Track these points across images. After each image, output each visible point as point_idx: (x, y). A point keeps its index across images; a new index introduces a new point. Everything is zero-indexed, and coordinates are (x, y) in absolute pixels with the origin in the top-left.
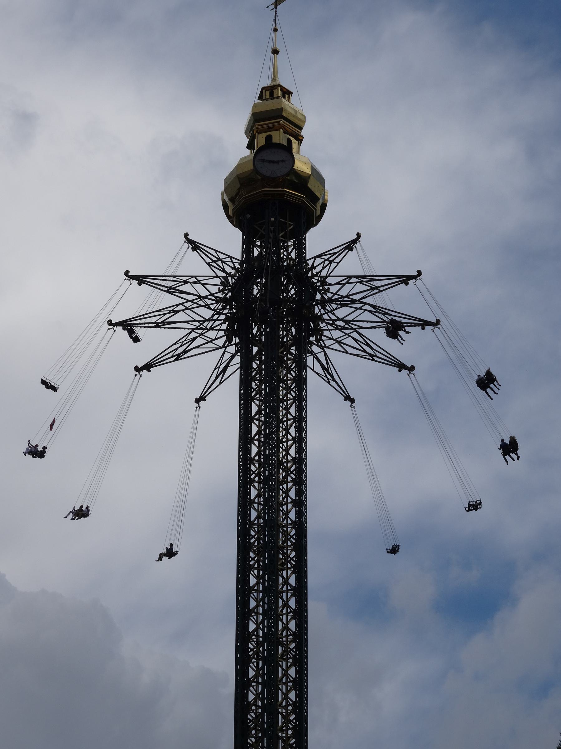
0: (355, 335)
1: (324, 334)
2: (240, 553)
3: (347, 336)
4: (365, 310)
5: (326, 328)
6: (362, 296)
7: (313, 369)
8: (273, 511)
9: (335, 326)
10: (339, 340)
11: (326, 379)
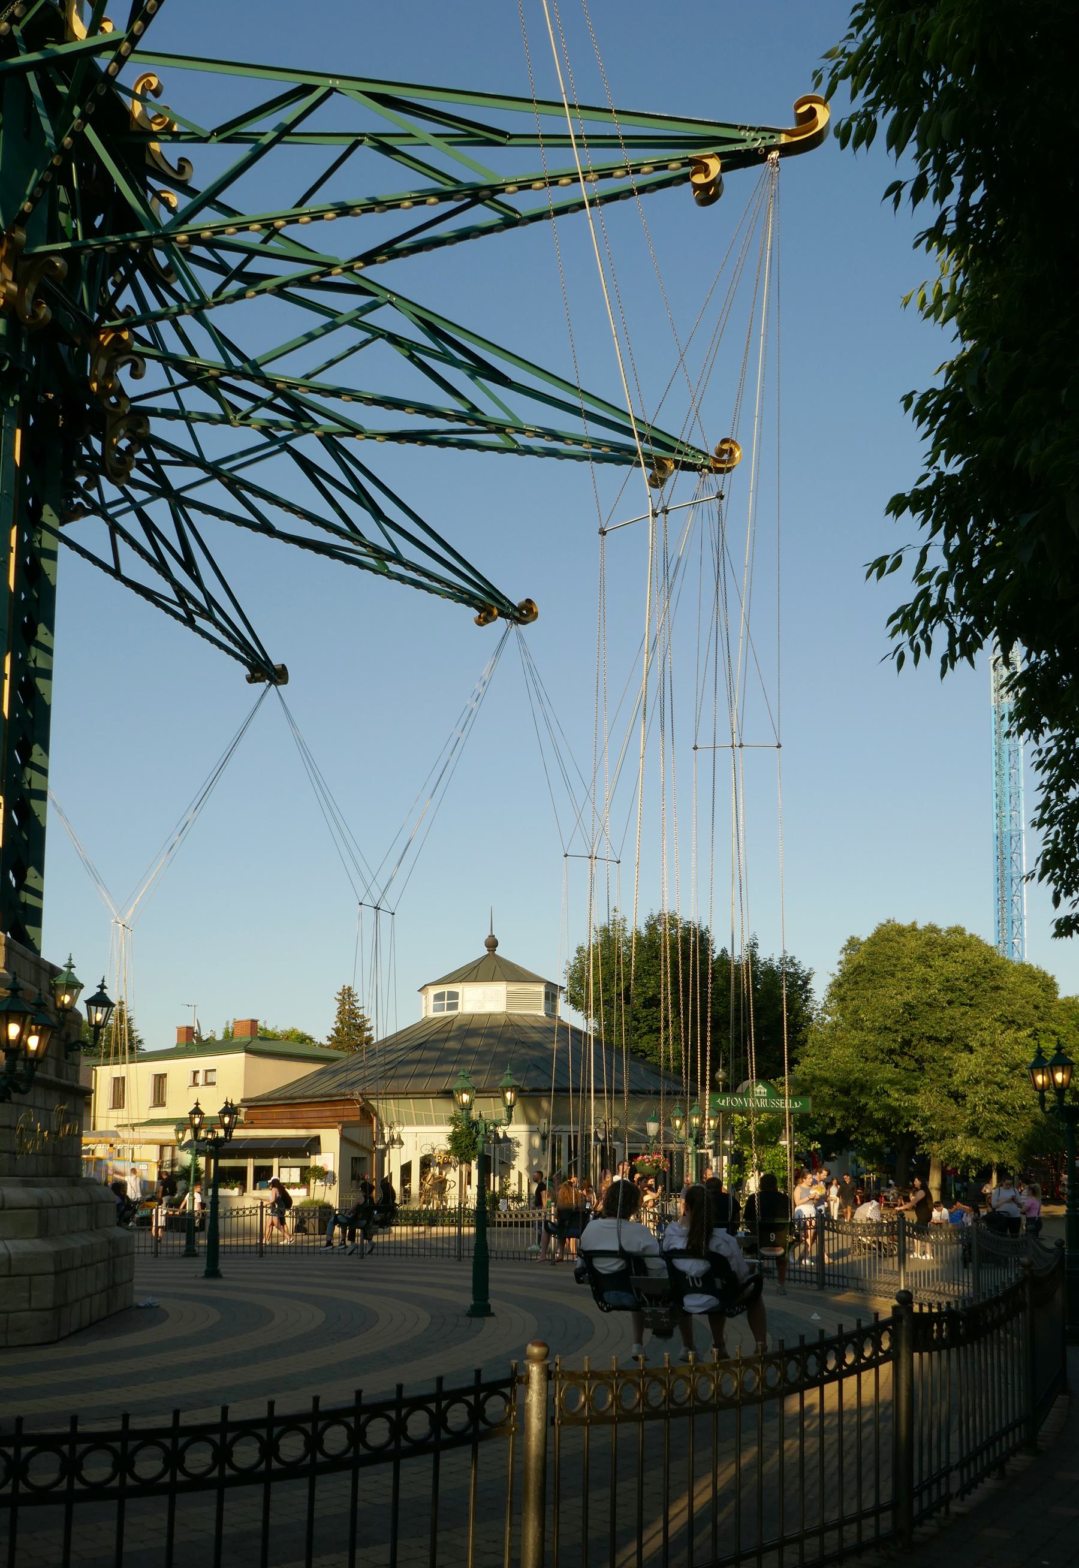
4: (377, 333)
5: (168, 402)
7: (113, 566)
11: (181, 611)
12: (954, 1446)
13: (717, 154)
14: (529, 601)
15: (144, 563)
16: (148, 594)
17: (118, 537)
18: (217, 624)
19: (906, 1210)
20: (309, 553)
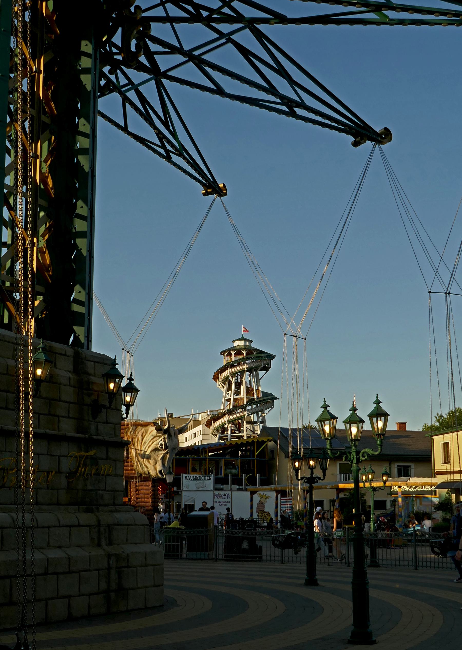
1: (100, 82)
2: (73, 242)
5: (159, 12)
9: (190, 8)
11: (162, 151)
12: (105, 473)
14: (386, 129)
17: (127, 105)
20: (318, 27)
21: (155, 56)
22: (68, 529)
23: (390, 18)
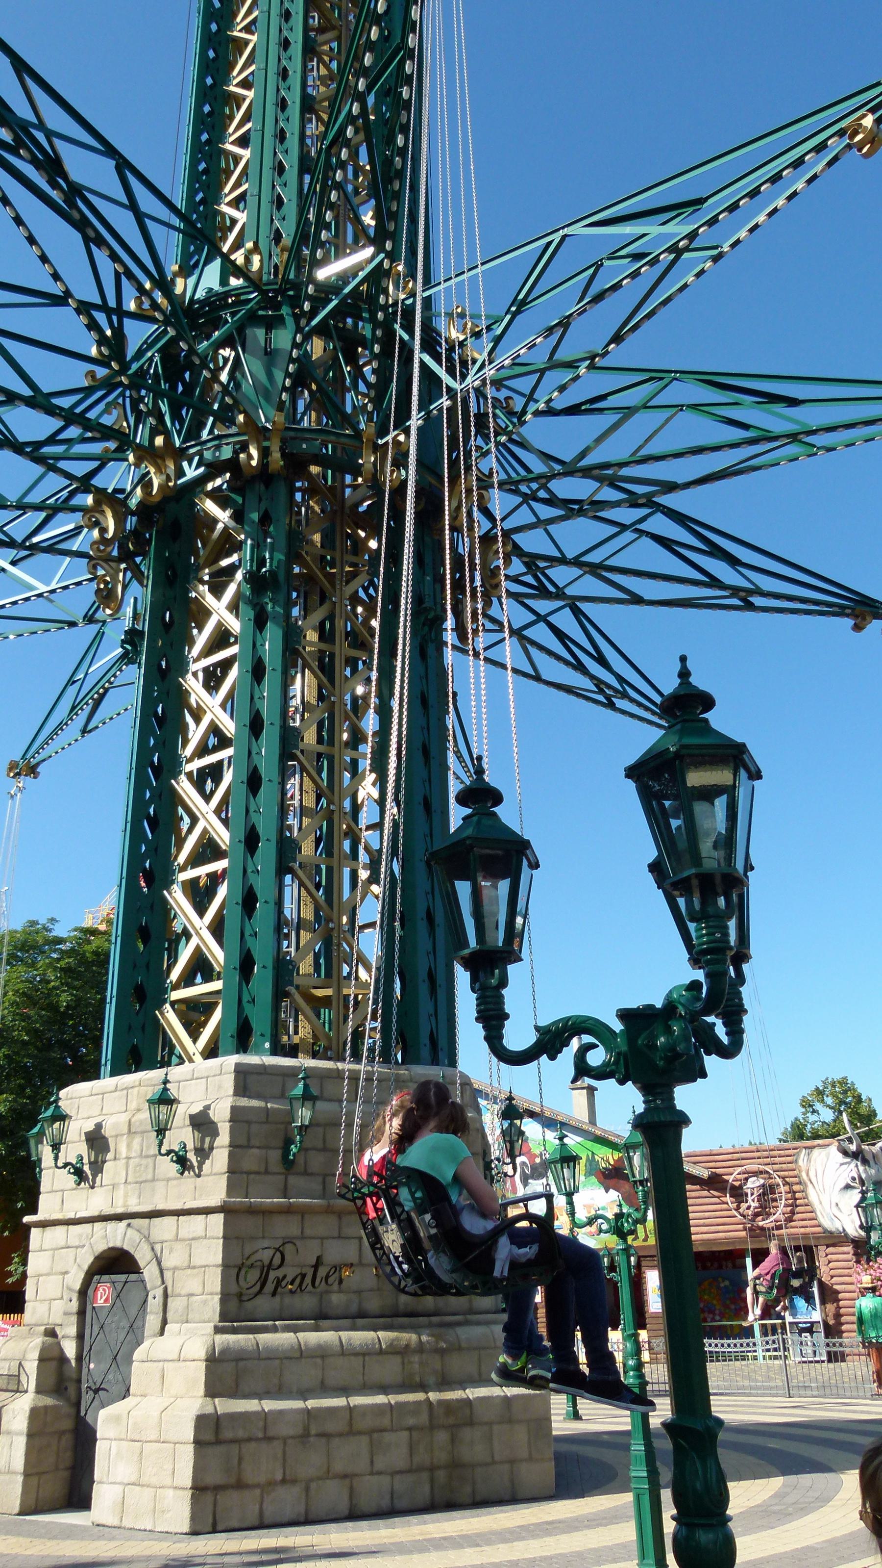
0: (660, 524)
3: (629, 536)
6: (137, 348)
8: (201, 208)
10: (594, 558)
11: (601, 698)
13: (868, 111)
15: (562, 666)
16: (569, 690)
18: (633, 700)
19: (253, 1238)
21: (62, 423)
22: (361, 1358)
23: (818, 446)
